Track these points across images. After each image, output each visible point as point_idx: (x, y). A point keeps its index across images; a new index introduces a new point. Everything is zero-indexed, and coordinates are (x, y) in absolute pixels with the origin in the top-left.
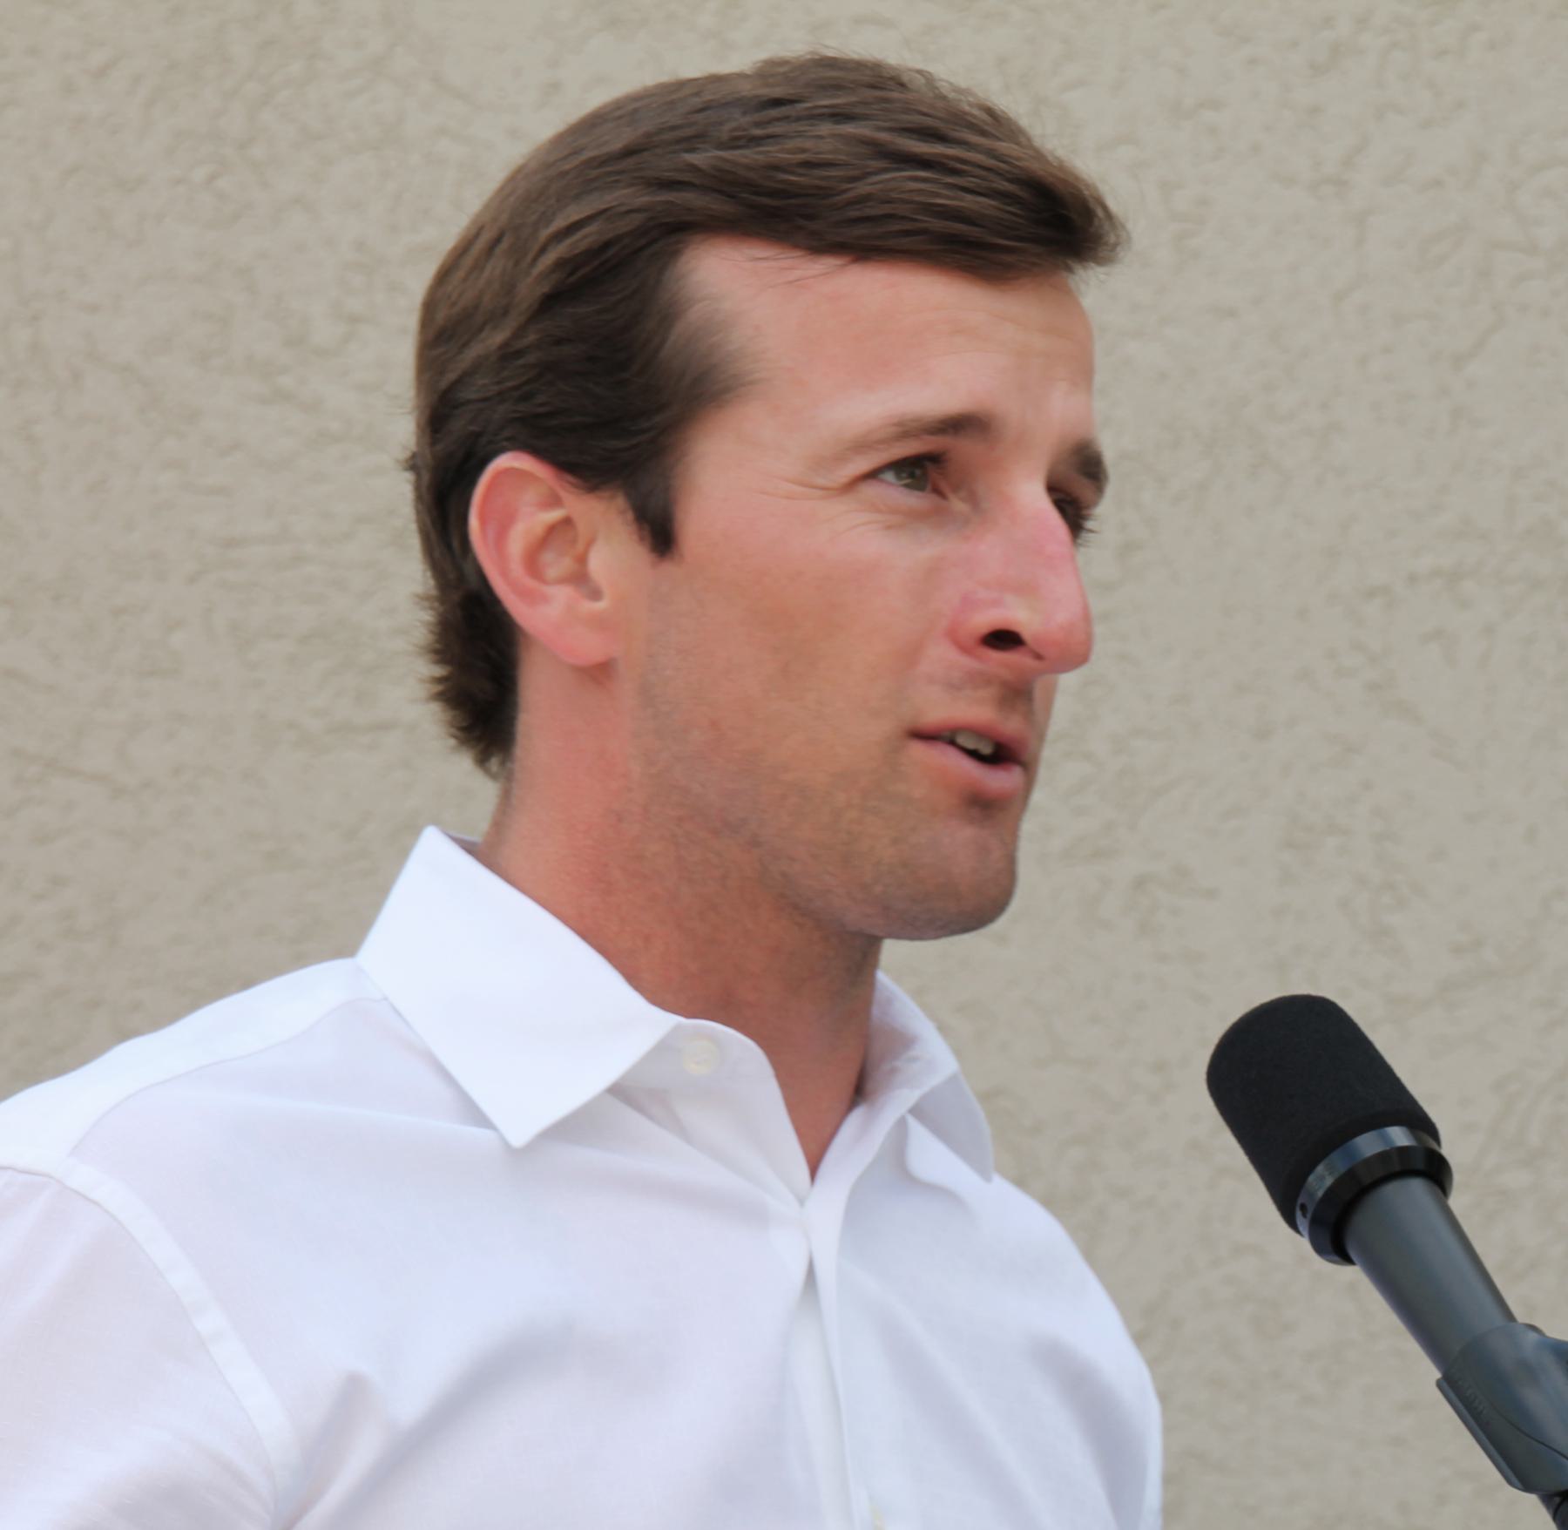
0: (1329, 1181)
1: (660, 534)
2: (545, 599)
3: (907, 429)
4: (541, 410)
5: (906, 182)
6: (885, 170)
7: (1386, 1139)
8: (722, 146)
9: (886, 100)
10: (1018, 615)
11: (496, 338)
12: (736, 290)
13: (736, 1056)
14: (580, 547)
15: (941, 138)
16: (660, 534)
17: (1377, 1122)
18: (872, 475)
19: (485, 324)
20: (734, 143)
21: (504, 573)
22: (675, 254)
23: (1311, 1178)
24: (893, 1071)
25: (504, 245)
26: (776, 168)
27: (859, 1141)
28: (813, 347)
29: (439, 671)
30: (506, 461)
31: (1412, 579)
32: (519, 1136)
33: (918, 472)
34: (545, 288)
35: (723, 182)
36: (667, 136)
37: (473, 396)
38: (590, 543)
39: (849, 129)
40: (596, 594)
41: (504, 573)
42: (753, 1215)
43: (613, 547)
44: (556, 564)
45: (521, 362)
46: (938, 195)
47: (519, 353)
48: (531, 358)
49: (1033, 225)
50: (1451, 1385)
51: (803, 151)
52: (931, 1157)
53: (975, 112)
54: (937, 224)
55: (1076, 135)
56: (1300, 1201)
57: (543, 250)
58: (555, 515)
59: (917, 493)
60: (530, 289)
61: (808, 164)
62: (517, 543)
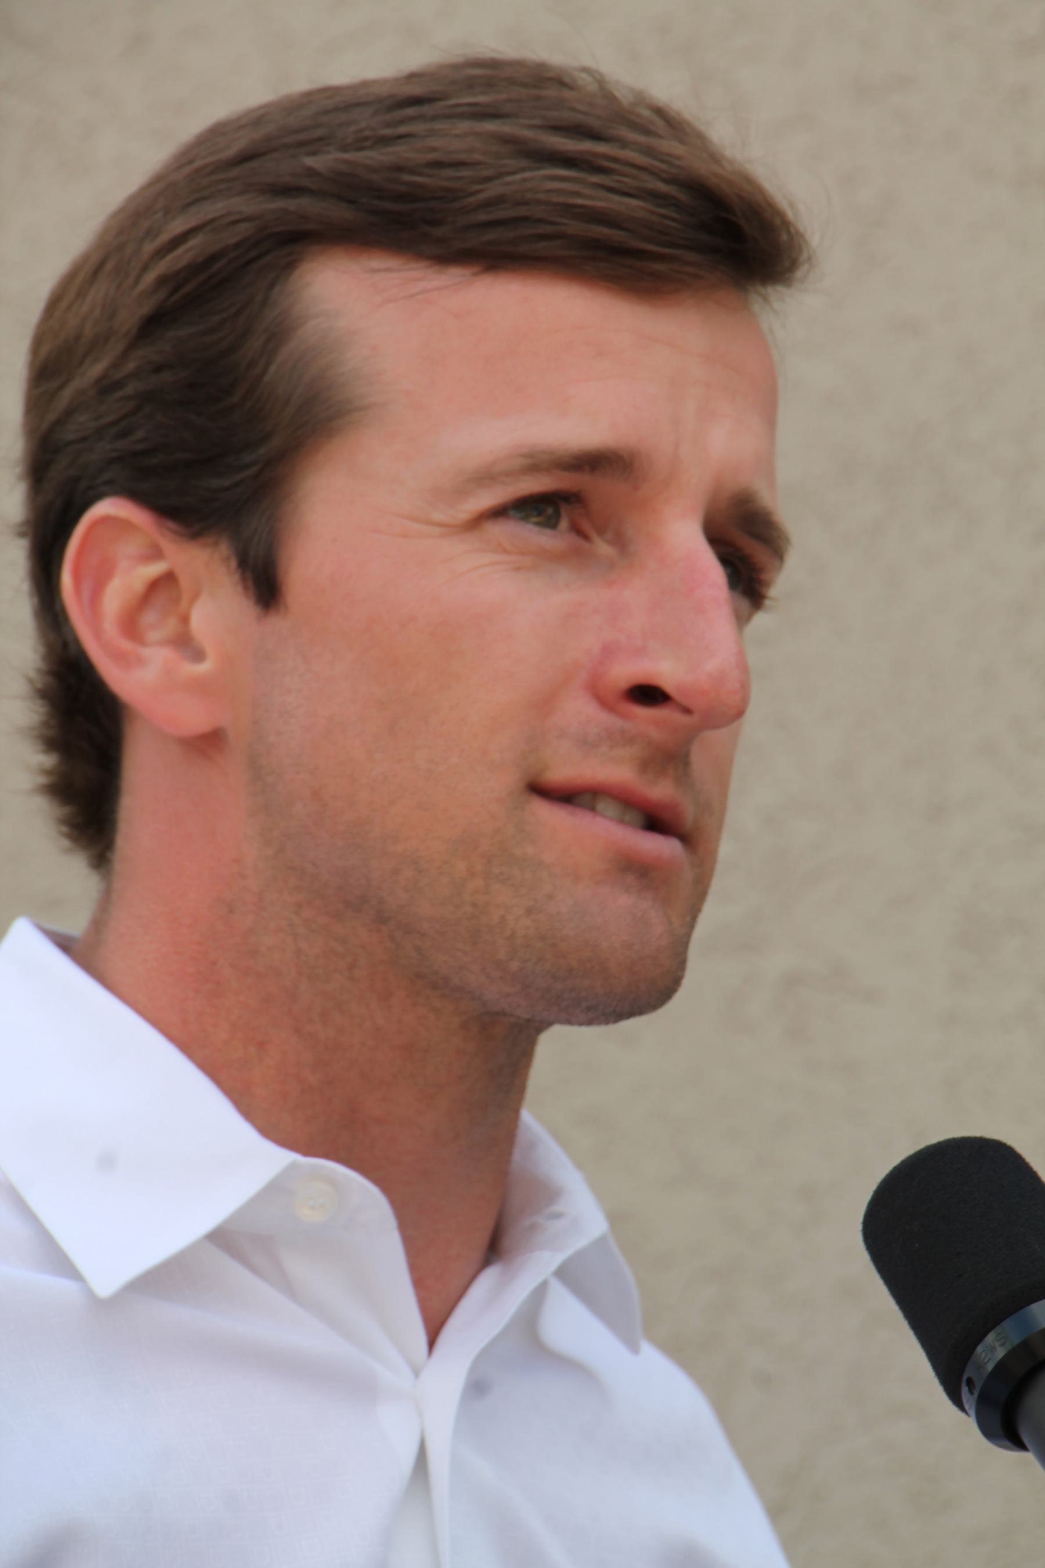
0: (1000, 1353)
1: (265, 585)
2: (140, 661)
3: (537, 462)
4: (140, 447)
5: (548, 182)
6: (523, 170)
8: (344, 148)
9: (538, 98)
10: (665, 670)
11: (95, 369)
12: (356, 307)
13: (354, 1203)
14: (184, 603)
15: (596, 136)
16: (265, 585)
18: (499, 513)
19: (85, 356)
20: (360, 143)
21: (98, 634)
22: (290, 266)
23: (979, 1349)
24: (533, 1227)
25: (109, 266)
26: (399, 169)
27: (487, 1308)
28: (439, 372)
30: (106, 508)
32: (105, 1285)
33: (550, 511)
34: (146, 308)
35: (345, 187)
36: (289, 140)
37: (71, 437)
38: (195, 596)
39: (490, 126)
40: (198, 655)
41: (98, 634)
42: (359, 1388)
43: (217, 603)
44: (157, 626)
45: (119, 394)
46: (577, 194)
47: (118, 385)
48: (130, 389)
49: (717, 239)
51: (434, 149)
52: (573, 1326)
53: (647, 113)
54: (574, 227)
55: (761, 133)
56: (965, 1378)
57: (145, 268)
58: (155, 569)
59: (548, 531)
60: (130, 315)
61: (438, 164)
62: (116, 595)
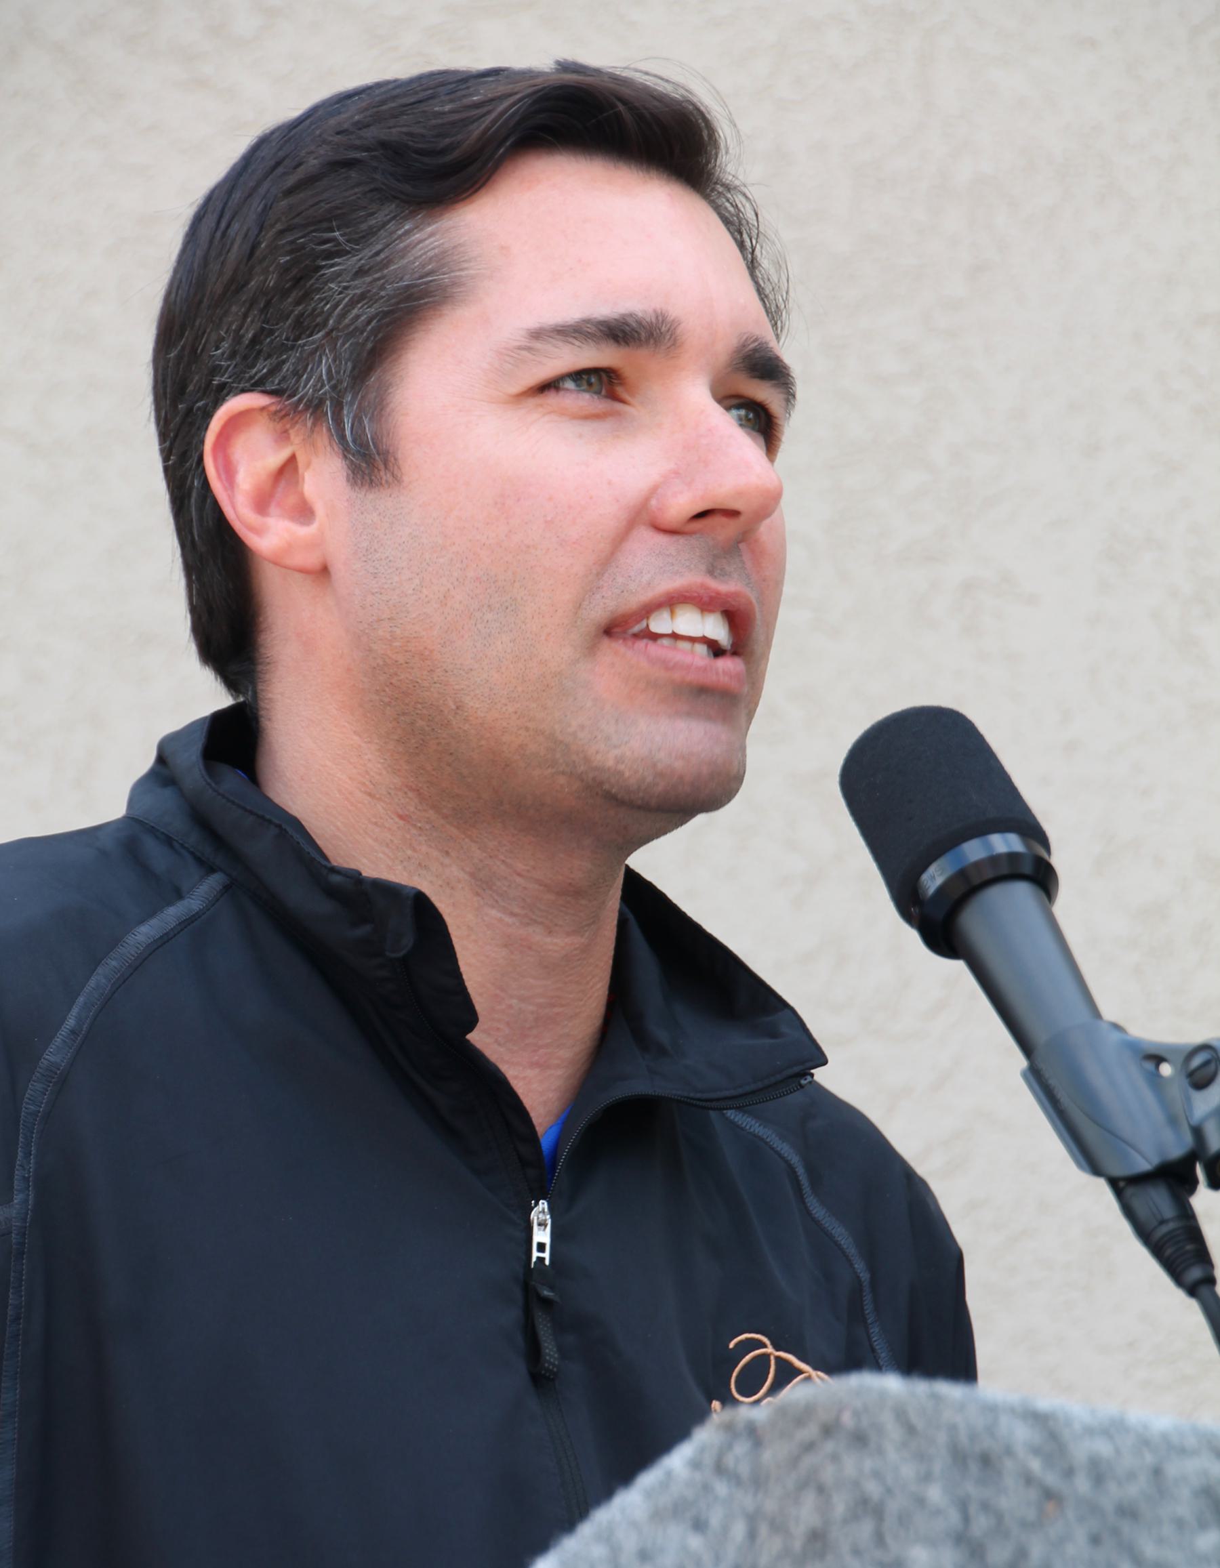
7: (989, 846)
17: (982, 829)
23: (925, 877)
29: (270, 695)
43: (324, 476)
49: (661, 138)
50: (1037, 1076)
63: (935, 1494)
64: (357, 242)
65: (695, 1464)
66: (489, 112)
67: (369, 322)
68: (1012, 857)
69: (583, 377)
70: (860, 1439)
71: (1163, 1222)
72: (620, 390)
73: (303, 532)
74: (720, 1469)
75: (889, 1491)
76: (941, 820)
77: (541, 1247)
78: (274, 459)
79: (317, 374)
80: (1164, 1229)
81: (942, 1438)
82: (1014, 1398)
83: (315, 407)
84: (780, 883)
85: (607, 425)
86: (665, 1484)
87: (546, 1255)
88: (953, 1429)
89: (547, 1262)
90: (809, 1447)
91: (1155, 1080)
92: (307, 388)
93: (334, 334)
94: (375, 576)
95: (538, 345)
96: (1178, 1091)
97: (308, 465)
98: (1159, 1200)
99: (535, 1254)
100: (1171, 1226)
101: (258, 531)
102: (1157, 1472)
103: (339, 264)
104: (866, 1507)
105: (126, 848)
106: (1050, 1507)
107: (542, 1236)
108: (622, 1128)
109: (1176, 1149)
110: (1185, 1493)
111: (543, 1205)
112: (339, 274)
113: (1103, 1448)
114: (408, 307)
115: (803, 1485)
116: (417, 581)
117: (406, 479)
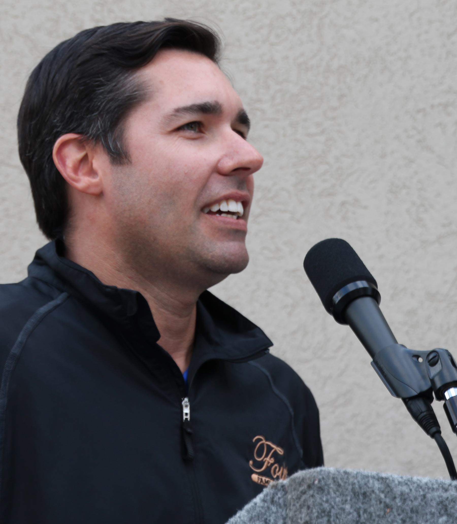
0: (339, 298)
7: (356, 285)
17: (361, 278)
23: (334, 297)
31: (432, 106)
43: (100, 161)
50: (376, 364)
63: (347, 507)
64: (108, 81)
65: (264, 501)
66: (151, 36)
67: (115, 108)
68: (364, 289)
69: (190, 126)
70: (321, 489)
71: (422, 413)
72: (202, 129)
73: (94, 180)
74: (273, 502)
75: (333, 507)
76: (338, 277)
77: (186, 414)
78: (79, 155)
79: (97, 125)
80: (423, 415)
81: (350, 487)
82: (374, 473)
83: (97, 138)
84: (272, 296)
85: (197, 142)
86: (254, 508)
87: (188, 417)
88: (353, 484)
89: (189, 420)
90: (304, 493)
91: (417, 364)
92: (92, 130)
93: (102, 113)
94: (123, 195)
95: (178, 114)
96: (425, 367)
97: (93, 158)
98: (420, 405)
99: (185, 417)
100: (425, 413)
101: (77, 181)
102: (424, 496)
103: (102, 89)
104: (323, 513)
105: (33, 284)
106: (388, 510)
107: (187, 410)
108: (210, 372)
109: (425, 386)
110: (434, 504)
111: (186, 399)
112: (102, 92)
113: (405, 489)
114: (128, 104)
115: (301, 507)
116: (139, 197)
117: (133, 161)
